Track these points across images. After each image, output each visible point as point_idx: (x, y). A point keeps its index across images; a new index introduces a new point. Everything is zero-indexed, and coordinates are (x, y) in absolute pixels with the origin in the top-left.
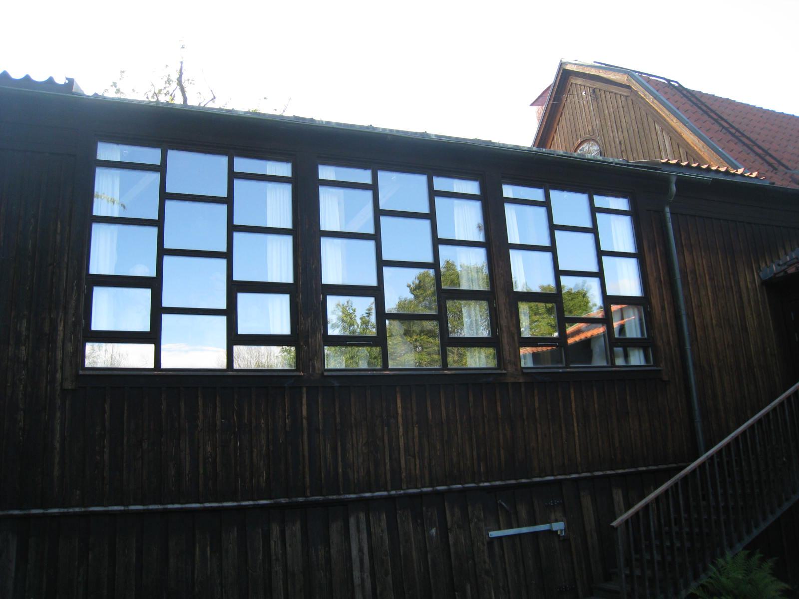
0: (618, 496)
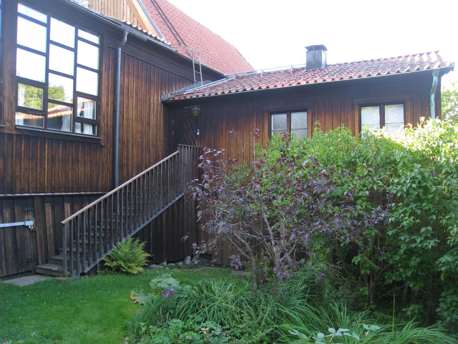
0: (67, 207)
